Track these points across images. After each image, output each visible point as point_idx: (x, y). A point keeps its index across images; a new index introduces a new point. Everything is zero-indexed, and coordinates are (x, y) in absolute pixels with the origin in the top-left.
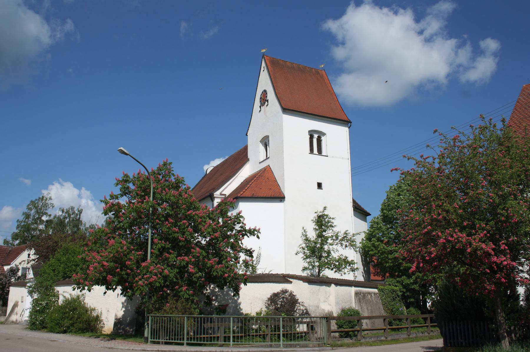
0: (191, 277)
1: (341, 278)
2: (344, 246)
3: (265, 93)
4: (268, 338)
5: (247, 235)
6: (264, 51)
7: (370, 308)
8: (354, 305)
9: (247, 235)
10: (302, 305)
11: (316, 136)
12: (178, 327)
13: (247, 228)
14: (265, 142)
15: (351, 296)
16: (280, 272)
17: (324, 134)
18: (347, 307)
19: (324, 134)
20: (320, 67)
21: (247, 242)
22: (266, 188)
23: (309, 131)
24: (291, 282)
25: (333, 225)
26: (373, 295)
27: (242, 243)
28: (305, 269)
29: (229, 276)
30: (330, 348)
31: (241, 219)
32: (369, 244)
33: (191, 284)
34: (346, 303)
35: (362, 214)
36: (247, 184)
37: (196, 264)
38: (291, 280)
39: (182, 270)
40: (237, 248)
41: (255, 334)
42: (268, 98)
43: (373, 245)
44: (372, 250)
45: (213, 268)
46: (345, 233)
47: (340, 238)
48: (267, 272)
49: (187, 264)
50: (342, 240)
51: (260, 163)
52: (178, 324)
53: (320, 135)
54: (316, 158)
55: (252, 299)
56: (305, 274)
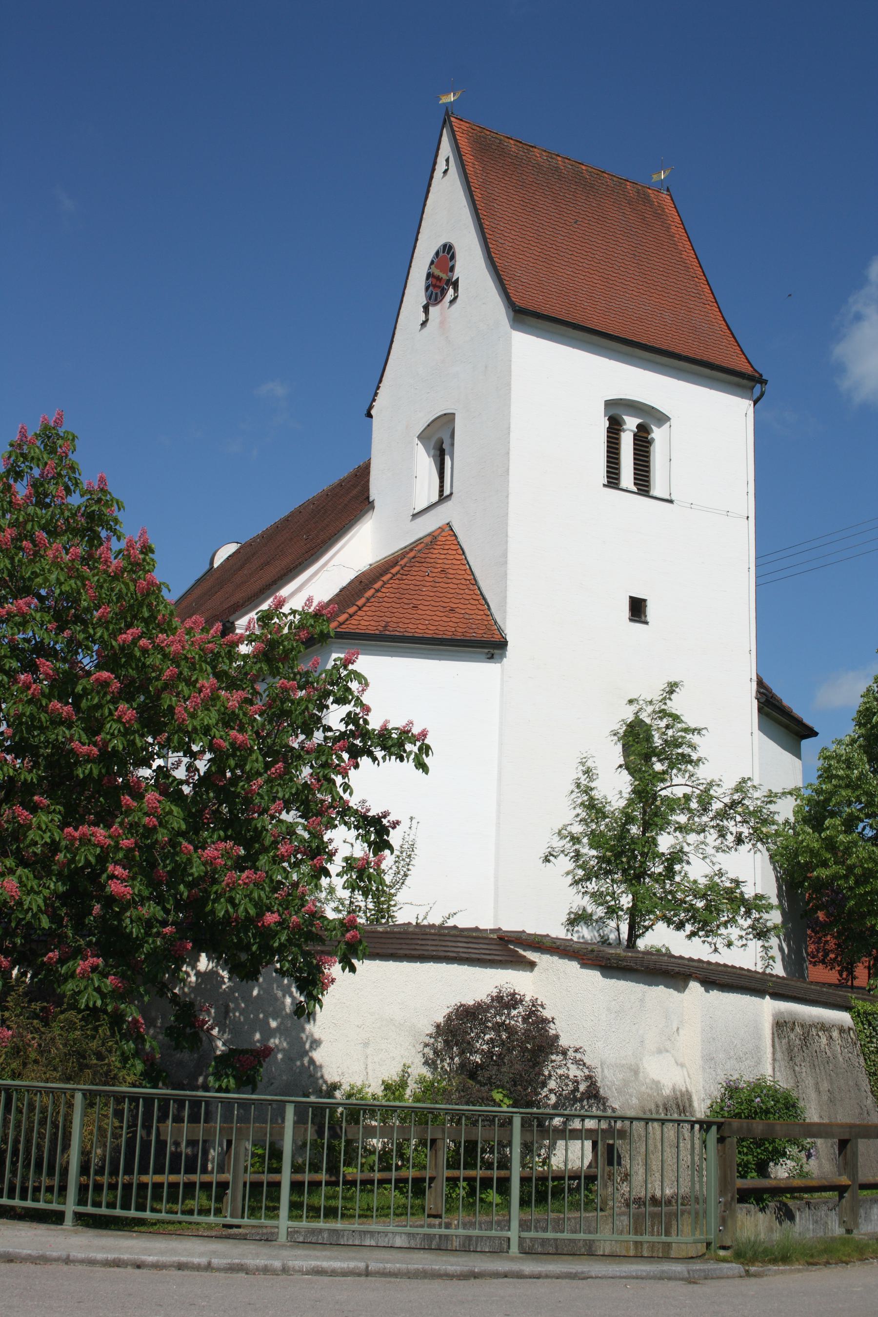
0: (119, 916)
1: (714, 958)
2: (730, 838)
3: (446, 255)
4: (433, 1199)
5: (370, 754)
6: (452, 98)
7: (825, 1086)
8: (765, 1066)
9: (370, 754)
10: (577, 1062)
11: (631, 423)
12: (41, 1136)
13: (375, 723)
14: (440, 440)
15: (757, 1034)
16: (486, 923)
17: (662, 419)
18: (750, 1077)
19: (662, 419)
20: (655, 178)
21: (371, 784)
22: (441, 608)
23: (610, 404)
24: (531, 965)
25: (695, 757)
26: (835, 1034)
27: (346, 787)
28: (577, 919)
29: (282, 923)
30: (736, 1268)
31: (354, 686)
32: (810, 838)
33: (116, 946)
34: (739, 1060)
35: (786, 727)
36: (367, 587)
37: (145, 862)
38: (531, 955)
39: (82, 887)
40: (322, 807)
41: (377, 1176)
42: (459, 272)
43: (830, 845)
44: (824, 864)
45: (214, 881)
46: (739, 788)
47: (717, 806)
48: (435, 919)
49: (102, 859)
50: (722, 815)
51: (415, 516)
52: (43, 1122)
53: (648, 421)
54: (626, 503)
55: (370, 1030)
56: (585, 933)
